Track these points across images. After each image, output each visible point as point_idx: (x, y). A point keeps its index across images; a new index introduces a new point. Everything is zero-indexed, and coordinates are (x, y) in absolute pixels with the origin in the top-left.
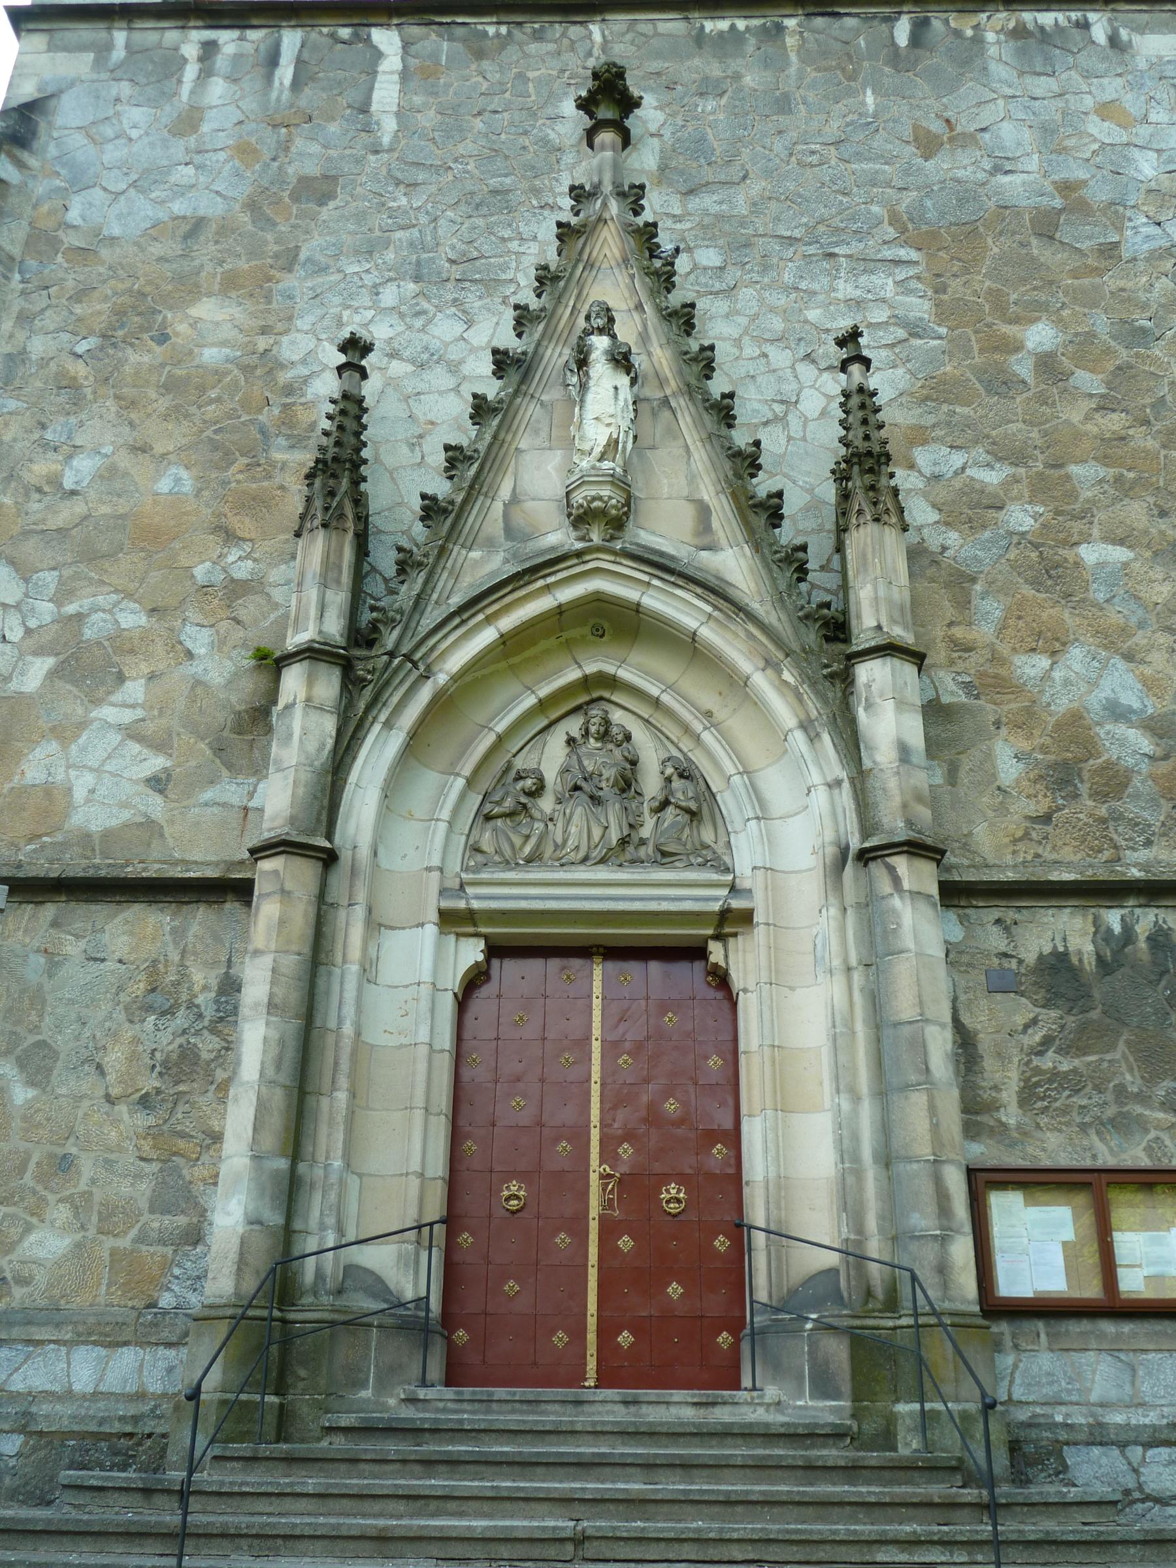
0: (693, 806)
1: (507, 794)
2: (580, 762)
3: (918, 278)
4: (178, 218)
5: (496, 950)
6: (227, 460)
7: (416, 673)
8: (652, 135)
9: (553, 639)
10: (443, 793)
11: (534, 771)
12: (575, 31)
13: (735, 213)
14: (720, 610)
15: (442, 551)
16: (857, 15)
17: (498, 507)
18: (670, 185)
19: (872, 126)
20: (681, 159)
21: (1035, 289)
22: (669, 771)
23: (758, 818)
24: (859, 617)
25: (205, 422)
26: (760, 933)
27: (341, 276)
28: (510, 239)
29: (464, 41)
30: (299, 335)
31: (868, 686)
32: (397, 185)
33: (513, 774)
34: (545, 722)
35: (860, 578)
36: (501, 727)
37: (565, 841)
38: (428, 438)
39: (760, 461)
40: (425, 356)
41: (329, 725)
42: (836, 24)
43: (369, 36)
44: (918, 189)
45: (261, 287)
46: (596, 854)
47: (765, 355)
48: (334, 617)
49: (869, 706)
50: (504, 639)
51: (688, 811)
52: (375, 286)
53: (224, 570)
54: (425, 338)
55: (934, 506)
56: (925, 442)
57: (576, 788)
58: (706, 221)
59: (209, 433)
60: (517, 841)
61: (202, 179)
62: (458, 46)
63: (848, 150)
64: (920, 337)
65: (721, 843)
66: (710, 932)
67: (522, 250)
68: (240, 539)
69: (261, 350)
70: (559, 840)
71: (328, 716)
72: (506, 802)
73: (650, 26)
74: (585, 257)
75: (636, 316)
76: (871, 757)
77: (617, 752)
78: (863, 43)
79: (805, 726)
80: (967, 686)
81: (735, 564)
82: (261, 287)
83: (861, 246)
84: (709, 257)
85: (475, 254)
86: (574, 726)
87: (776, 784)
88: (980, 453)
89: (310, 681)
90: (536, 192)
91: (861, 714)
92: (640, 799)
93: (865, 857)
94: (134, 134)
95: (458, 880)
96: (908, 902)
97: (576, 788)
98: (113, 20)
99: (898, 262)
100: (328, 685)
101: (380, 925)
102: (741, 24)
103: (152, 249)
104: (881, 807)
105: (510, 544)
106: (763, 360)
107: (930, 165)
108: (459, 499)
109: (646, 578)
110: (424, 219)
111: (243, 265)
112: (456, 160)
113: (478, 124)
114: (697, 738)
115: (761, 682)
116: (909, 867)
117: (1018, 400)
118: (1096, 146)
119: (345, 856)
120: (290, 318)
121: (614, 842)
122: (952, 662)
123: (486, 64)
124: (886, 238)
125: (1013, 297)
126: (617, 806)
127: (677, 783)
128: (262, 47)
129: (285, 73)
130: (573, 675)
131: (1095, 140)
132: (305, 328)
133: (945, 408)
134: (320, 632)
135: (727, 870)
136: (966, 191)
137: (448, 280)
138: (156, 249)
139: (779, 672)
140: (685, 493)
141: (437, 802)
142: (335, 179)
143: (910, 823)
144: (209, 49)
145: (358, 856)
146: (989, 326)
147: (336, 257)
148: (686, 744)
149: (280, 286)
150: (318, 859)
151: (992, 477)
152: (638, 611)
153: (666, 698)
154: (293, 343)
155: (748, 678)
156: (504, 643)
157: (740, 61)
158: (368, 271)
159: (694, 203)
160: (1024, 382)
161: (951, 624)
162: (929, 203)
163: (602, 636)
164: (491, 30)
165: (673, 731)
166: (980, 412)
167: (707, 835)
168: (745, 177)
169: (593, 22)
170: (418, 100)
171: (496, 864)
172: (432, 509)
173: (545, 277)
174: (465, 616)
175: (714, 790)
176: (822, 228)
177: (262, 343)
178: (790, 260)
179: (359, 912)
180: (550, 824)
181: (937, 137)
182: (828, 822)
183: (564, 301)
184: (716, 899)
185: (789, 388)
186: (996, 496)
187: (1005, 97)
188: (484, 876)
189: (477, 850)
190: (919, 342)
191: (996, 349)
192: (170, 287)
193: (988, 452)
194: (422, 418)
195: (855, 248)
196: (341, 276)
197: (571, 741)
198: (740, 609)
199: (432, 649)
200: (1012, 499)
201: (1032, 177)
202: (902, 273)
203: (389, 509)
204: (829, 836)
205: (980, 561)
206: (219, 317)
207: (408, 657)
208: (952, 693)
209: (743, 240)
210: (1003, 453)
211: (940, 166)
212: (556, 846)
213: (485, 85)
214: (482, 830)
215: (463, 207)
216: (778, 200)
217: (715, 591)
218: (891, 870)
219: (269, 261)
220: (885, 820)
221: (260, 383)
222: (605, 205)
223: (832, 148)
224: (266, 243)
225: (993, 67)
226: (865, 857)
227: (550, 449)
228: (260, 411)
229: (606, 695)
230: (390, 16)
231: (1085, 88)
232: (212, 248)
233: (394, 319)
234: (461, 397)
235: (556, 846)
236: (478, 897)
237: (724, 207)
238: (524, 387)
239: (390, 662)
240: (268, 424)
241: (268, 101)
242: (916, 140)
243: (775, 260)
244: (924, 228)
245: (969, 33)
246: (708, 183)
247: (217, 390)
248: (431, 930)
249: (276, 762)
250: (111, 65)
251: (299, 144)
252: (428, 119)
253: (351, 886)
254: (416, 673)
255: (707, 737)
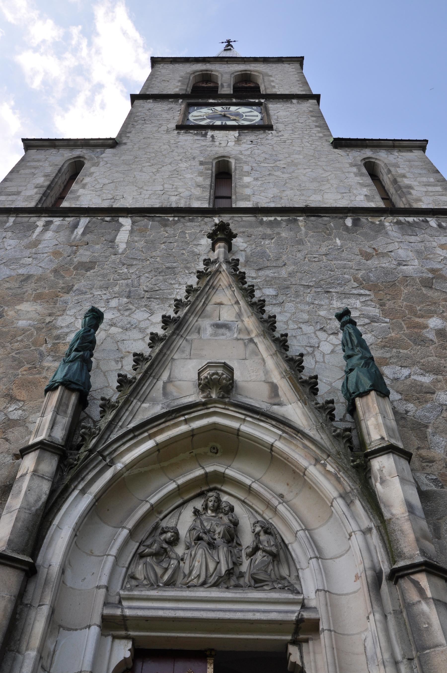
0: (274, 549)
1: (155, 541)
2: (202, 523)
3: (371, 301)
4: (20, 275)
5: (140, 653)
6: (20, 364)
7: (104, 463)
8: (241, 251)
9: (188, 453)
10: (114, 538)
11: (172, 528)
12: (206, 220)
13: (281, 276)
14: (287, 433)
15: (127, 402)
16: (328, 217)
17: (160, 384)
18: (250, 267)
19: (341, 249)
20: (255, 258)
21: (428, 305)
22: (258, 529)
23: (316, 557)
24: (369, 434)
25: (12, 349)
26: (324, 637)
27: (92, 295)
28: (174, 284)
29: (159, 221)
30: (67, 317)
31: (381, 470)
32: (123, 265)
33: (159, 531)
34: (180, 501)
35: (367, 415)
36: (154, 500)
37: (191, 572)
38: (126, 359)
39: (303, 364)
40: (129, 326)
41: (46, 487)
42: (320, 220)
43: (118, 220)
44: (365, 270)
45: (53, 299)
46: (212, 580)
47: (300, 328)
48: (60, 430)
49: (383, 482)
50: (159, 447)
51: (270, 553)
52: (107, 299)
53: (6, 415)
54: (129, 319)
55: (397, 392)
56: (387, 364)
57: (199, 538)
58: (268, 279)
59: (13, 354)
60: (159, 571)
61: (34, 262)
62: (157, 223)
63: (329, 257)
64: (376, 322)
65: (293, 577)
66: (289, 638)
67: (180, 287)
68: (18, 400)
69: (47, 322)
70: (187, 572)
71: (45, 482)
72: (154, 546)
73: (240, 218)
74: (211, 284)
75: (236, 307)
76: (389, 511)
77: (226, 519)
78: (332, 225)
79: (343, 496)
80: (435, 481)
81: (295, 411)
82: (53, 299)
83: (342, 289)
84: (270, 291)
85: (157, 289)
86: (199, 504)
87: (327, 536)
88: (416, 369)
89: (39, 461)
90: (188, 268)
91: (379, 487)
92: (240, 548)
93: (396, 576)
94: (9, 248)
95: (117, 598)
96: (433, 606)
97: (199, 538)
98: (10, 214)
99: (361, 295)
100: (49, 465)
101: (60, 626)
102: (279, 219)
103: (5, 285)
104: (401, 542)
105: (165, 401)
106: (300, 330)
107: (369, 262)
108: (139, 377)
109: (243, 417)
110: (134, 276)
111: (46, 291)
112: (151, 258)
113: (163, 246)
114: (275, 510)
115: (314, 472)
116: (429, 581)
117: (431, 347)
118: (442, 258)
119: (43, 573)
120: (64, 310)
121: (223, 572)
122: (423, 468)
123: (167, 228)
124: (354, 286)
125: (418, 308)
126: (225, 549)
127: (263, 537)
128: (71, 222)
129: (80, 230)
130: (199, 472)
131: (441, 256)
132: (71, 314)
133: (394, 350)
134: (50, 436)
135: (298, 593)
136: (388, 271)
137: (143, 298)
138: (7, 285)
139: (324, 466)
140: (263, 379)
141: (109, 544)
142: (95, 263)
143: (423, 552)
144: (48, 225)
145: (51, 571)
146: (410, 318)
147: (91, 289)
148: (268, 515)
149: (62, 299)
150: (23, 570)
151: (427, 379)
152: (238, 435)
153: (255, 486)
154: (63, 319)
155: (306, 469)
156: (158, 450)
157: (279, 229)
158: (105, 294)
159: (261, 273)
160: (431, 340)
161: (418, 448)
162: (371, 275)
163: (216, 453)
164: (171, 219)
165: (260, 507)
166: (413, 352)
167: (284, 572)
168: (285, 265)
169: (215, 217)
170: (136, 239)
171: (144, 585)
172: (123, 381)
173: (190, 290)
174: (137, 433)
175: (287, 542)
176: (322, 282)
177: (48, 319)
178: (309, 293)
179: (45, 610)
180: (182, 563)
181: (370, 253)
182: (365, 554)
183: (200, 299)
184: (293, 612)
185: (314, 341)
186: (429, 388)
187: (398, 242)
188: (136, 593)
189: (133, 577)
190: (376, 324)
191: (415, 327)
192: (9, 298)
193: (421, 369)
194: (124, 350)
195: (339, 289)
196: (92, 295)
197: (196, 512)
198: (298, 431)
199: (115, 450)
200: (439, 389)
201: (416, 267)
202: (363, 299)
203: (101, 389)
204: (368, 564)
205: (428, 418)
206: (29, 309)
207: (100, 453)
208: (427, 485)
209: (286, 286)
210: (427, 369)
211: (373, 263)
212: (185, 576)
213: (167, 235)
214: (138, 564)
215: (153, 273)
216: (301, 272)
217: (283, 423)
218: (416, 584)
219: (59, 290)
220: (406, 550)
221: (44, 334)
222: (220, 266)
223: (324, 256)
224: (59, 283)
225: (390, 233)
226: (396, 576)
227: (190, 359)
228: (41, 346)
229: (219, 486)
230: (128, 214)
231: (431, 239)
232: (33, 285)
233: (115, 312)
234: (145, 342)
235: (185, 576)
236: (130, 608)
237: (276, 274)
238: (178, 332)
239: (89, 456)
240: (45, 351)
241: (70, 238)
242: (361, 254)
243: (302, 293)
244: (371, 283)
245: (378, 223)
246: (267, 267)
247: (22, 337)
248: (95, 630)
249: (8, 507)
250: (5, 227)
251: (81, 251)
252: (141, 244)
253: (43, 592)
254: (104, 463)
255: (281, 508)
